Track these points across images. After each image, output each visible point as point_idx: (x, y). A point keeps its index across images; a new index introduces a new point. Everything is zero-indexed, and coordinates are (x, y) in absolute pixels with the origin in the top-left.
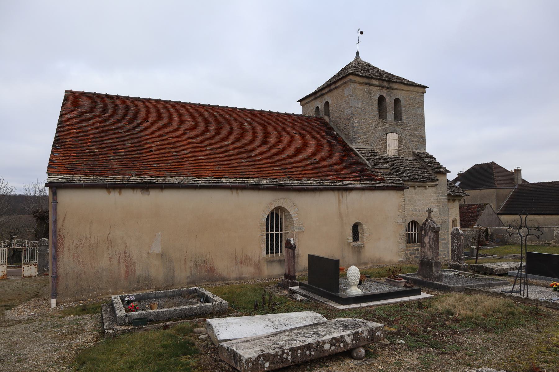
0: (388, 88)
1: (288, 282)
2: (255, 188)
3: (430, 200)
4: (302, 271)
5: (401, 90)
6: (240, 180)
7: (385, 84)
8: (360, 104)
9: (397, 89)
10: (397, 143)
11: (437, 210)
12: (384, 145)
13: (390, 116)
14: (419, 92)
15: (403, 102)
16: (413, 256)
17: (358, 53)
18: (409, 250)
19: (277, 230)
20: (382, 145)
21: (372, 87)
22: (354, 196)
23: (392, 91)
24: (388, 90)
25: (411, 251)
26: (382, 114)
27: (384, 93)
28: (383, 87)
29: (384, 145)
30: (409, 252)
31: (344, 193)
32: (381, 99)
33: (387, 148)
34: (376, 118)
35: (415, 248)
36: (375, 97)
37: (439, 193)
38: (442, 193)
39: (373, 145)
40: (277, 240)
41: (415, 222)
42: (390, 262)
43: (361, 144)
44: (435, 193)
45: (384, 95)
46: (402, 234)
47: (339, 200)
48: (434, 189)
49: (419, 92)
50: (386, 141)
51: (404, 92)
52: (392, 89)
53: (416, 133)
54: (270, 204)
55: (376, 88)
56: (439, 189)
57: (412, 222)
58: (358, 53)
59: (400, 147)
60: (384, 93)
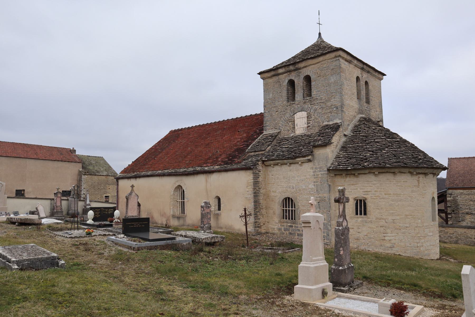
0: (295, 70)
1: (439, 280)
2: (170, 175)
3: (306, 176)
4: (188, 226)
5: (309, 65)
6: (166, 171)
7: (291, 68)
8: (271, 95)
9: (303, 67)
10: (306, 120)
11: (313, 187)
12: (292, 126)
13: (299, 96)
14: (331, 59)
15: (313, 77)
16: (288, 232)
17: (320, 34)
18: (283, 226)
19: (292, 208)
20: (290, 127)
21: (281, 76)
22: (214, 177)
23: (300, 71)
24: (296, 72)
25: (285, 227)
26: (292, 96)
27: (293, 76)
28: (290, 71)
29: (292, 126)
30: (283, 227)
31: (209, 175)
32: (292, 83)
33: (295, 128)
34: (284, 103)
35: (289, 224)
36: (284, 84)
37: (316, 168)
38: (320, 168)
39: (281, 128)
40: (286, 216)
41: (289, 198)
42: (239, 230)
43: (270, 130)
44: (312, 168)
45: (293, 78)
46: (250, 208)
47: (206, 180)
48: (310, 164)
49: (331, 59)
50: (294, 121)
51: (313, 66)
52: (300, 69)
53: (329, 104)
54: (175, 183)
55: (284, 75)
56: (317, 164)
57: (286, 199)
58: (320, 34)
59: (308, 123)
60: (293, 76)
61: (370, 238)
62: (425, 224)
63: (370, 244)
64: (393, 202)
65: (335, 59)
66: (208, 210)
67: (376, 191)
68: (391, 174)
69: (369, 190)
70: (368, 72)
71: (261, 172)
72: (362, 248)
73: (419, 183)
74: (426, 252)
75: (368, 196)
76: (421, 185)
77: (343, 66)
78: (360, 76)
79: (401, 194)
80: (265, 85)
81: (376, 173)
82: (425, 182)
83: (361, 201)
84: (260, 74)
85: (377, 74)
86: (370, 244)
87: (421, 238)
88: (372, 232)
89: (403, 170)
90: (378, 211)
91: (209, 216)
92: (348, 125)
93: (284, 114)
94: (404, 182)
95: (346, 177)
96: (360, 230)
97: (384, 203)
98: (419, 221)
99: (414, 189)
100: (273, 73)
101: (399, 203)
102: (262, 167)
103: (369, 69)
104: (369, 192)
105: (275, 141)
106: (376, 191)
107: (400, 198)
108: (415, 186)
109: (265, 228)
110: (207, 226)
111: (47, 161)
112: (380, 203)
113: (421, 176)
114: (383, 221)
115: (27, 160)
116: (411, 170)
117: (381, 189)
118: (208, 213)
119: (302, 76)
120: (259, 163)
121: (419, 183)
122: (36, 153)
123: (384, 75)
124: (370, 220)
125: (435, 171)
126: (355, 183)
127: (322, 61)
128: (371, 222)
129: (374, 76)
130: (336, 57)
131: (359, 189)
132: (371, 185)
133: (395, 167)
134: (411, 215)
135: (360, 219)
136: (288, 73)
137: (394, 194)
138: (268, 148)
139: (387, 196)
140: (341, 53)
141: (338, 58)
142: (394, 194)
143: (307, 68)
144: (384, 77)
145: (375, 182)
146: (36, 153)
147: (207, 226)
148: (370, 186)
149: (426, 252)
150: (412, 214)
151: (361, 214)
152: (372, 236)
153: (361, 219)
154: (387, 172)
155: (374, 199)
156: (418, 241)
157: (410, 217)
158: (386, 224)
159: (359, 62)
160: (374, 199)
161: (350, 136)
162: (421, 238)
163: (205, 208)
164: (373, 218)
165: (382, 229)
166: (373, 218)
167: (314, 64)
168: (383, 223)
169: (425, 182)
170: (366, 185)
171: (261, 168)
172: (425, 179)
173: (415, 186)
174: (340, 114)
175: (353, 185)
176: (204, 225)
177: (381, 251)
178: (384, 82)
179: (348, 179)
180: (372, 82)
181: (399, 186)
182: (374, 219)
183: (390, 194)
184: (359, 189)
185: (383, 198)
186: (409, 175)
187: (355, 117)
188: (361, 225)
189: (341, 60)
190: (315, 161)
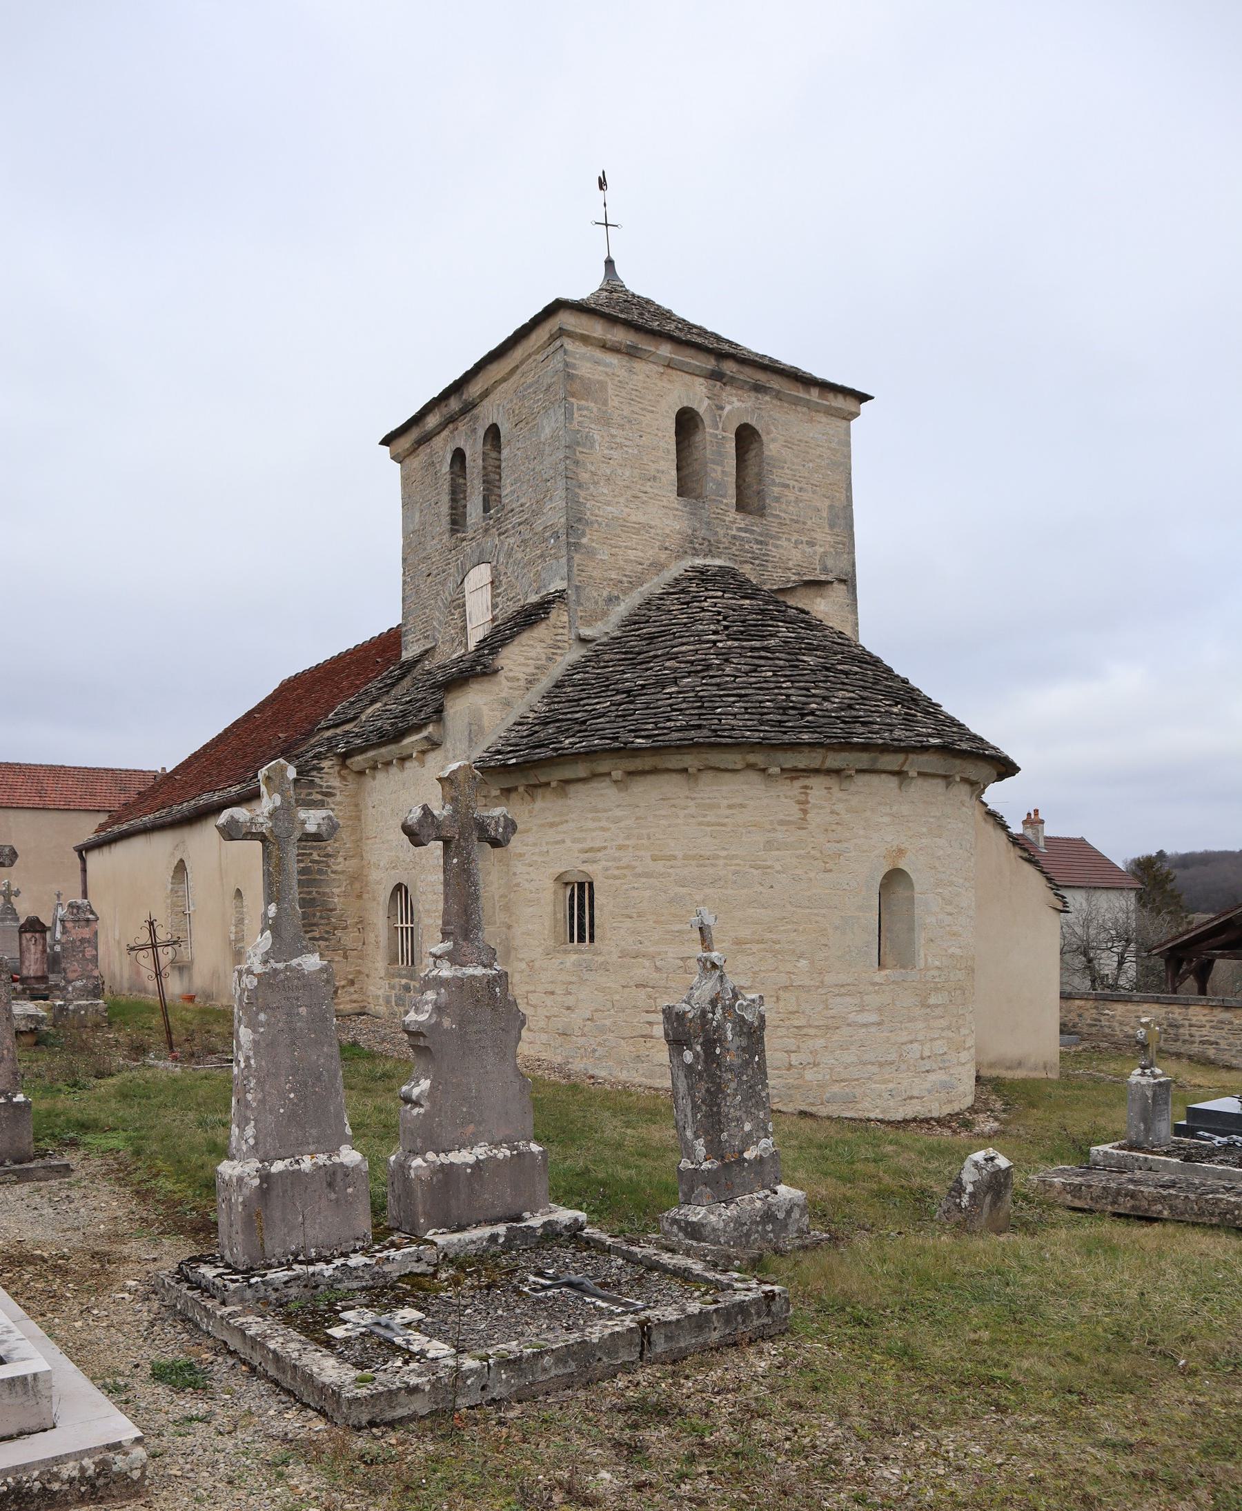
15: (504, 430)
17: (609, 263)
23: (475, 411)
51: (504, 385)
54: (173, 854)
58: (609, 263)
61: (602, 1030)
62: (829, 979)
63: (600, 1051)
64: (684, 890)
65: (551, 348)
66: (86, 933)
67: (620, 848)
68: (676, 777)
69: (598, 844)
70: (758, 388)
71: (338, 798)
72: (577, 1065)
73: (805, 812)
74: (836, 1088)
75: (595, 866)
76: (814, 818)
77: (584, 369)
78: (702, 407)
79: (717, 857)
80: (406, 481)
81: (617, 775)
82: (839, 807)
83: (581, 885)
84: (386, 441)
85: (814, 394)
86: (600, 1051)
87: (812, 1031)
88: (609, 1005)
89: (715, 758)
90: (628, 923)
91: (89, 952)
92: (611, 600)
93: (443, 583)
94: (730, 807)
95: (533, 799)
96: (570, 1001)
97: (647, 893)
98: (803, 963)
99: (779, 835)
100: (414, 434)
101: (708, 891)
102: (343, 778)
103: (762, 377)
104: (599, 850)
105: (406, 682)
106: (620, 848)
107: (711, 871)
108: (782, 823)
109: (355, 997)
110: (79, 984)
111: (74, 814)
112: (634, 893)
113: (818, 785)
114: (647, 963)
115: (11, 813)
116: (757, 758)
117: (639, 837)
118: (82, 941)
119: (481, 433)
120: (326, 764)
121: (805, 812)
122: (40, 793)
123: (864, 398)
124: (600, 959)
125: (974, 770)
126: (557, 819)
127: (522, 363)
128: (605, 967)
129: (796, 401)
130: (553, 338)
131: (568, 843)
132: (604, 823)
133: (679, 748)
134: (761, 942)
135: (575, 956)
136: (451, 426)
137: (686, 857)
138: (370, 710)
139: (659, 866)
140: (566, 320)
141: (558, 343)
142: (686, 857)
143: (492, 396)
144: (864, 406)
145: (618, 813)
146: (40, 793)
147: (79, 984)
148: (603, 829)
149: (836, 1088)
150: (768, 936)
151: (581, 939)
152: (608, 1022)
153: (574, 957)
154: (654, 771)
155: (616, 877)
156: (791, 1043)
157: (755, 947)
158: (656, 975)
159: (691, 352)
160: (616, 877)
161: (605, 639)
162: (812, 1031)
163: (69, 925)
164: (610, 953)
165: (642, 994)
166: (610, 953)
167: (504, 380)
168: (642, 970)
169: (839, 807)
170: (590, 824)
171: (336, 782)
172: (841, 795)
173: (782, 823)
174: (564, 560)
175: (552, 825)
176: (69, 982)
177: (638, 1079)
178: (865, 428)
179: (539, 804)
180: (786, 431)
181: (709, 824)
182: (614, 957)
183: (674, 857)
184: (568, 843)
185: (647, 875)
186: (754, 777)
187: (658, 567)
188: (574, 979)
189: (569, 345)
190: (448, 745)
